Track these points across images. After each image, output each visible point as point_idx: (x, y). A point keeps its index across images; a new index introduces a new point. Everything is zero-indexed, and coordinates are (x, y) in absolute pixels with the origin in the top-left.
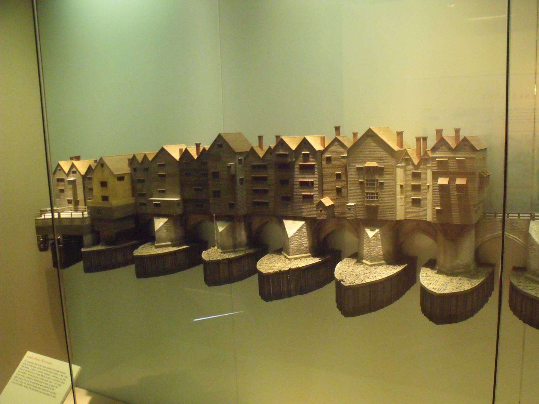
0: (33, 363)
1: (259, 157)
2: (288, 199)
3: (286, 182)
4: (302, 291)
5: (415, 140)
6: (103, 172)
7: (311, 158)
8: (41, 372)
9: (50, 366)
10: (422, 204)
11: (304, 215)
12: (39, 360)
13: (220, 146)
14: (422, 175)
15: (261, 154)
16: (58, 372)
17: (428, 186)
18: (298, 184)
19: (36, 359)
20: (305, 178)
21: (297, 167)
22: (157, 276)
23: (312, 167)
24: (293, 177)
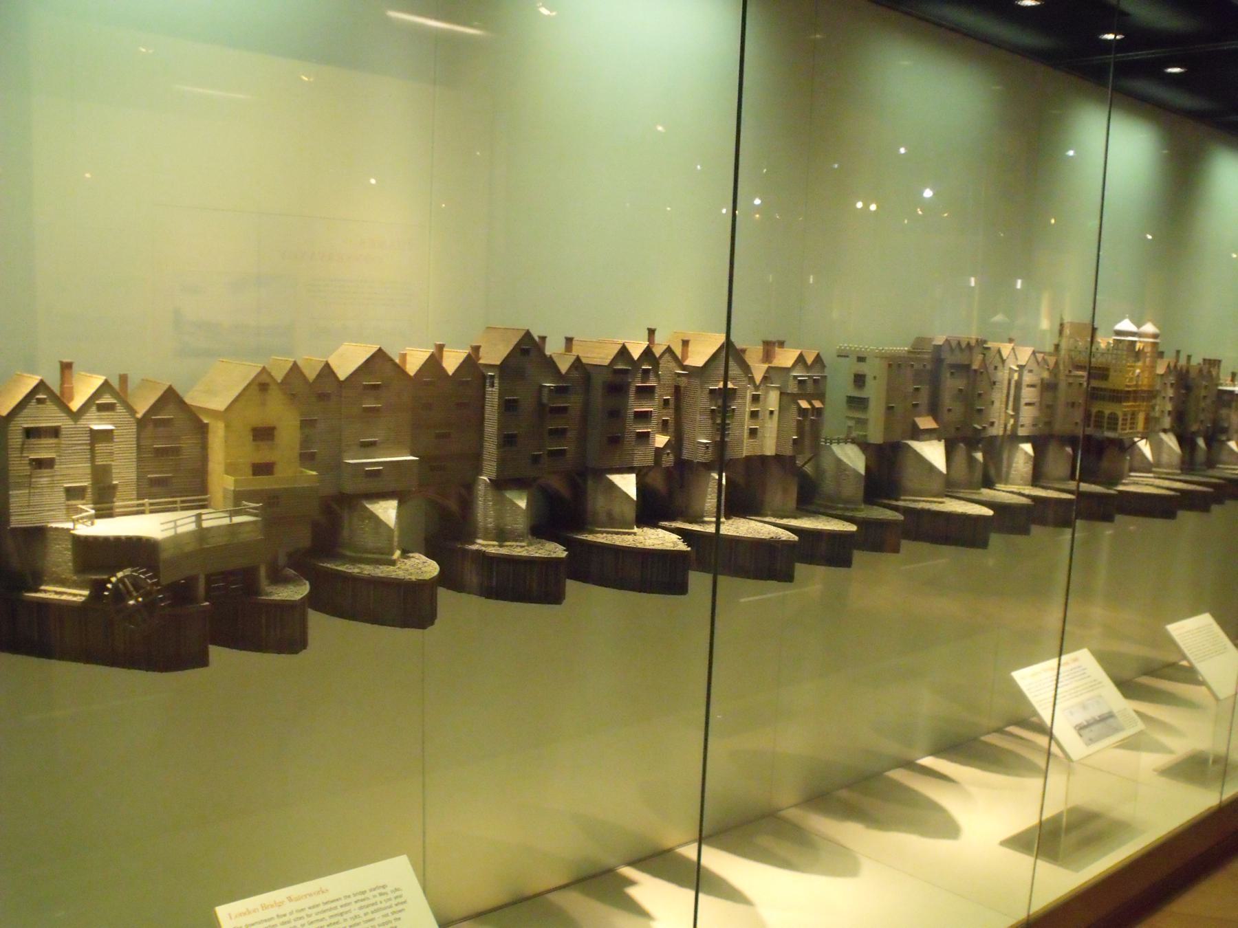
0: (272, 919)
1: (558, 371)
2: (615, 441)
3: (616, 414)
4: (644, 586)
5: (564, 341)
6: (263, 404)
7: (652, 377)
8: (322, 920)
9: (328, 897)
10: (759, 434)
11: (636, 464)
12: (279, 905)
13: (525, 352)
14: (762, 398)
15: (564, 367)
16: (364, 893)
17: (772, 412)
18: (632, 416)
19: (264, 907)
20: (642, 406)
21: (632, 390)
22: (229, 647)
23: (651, 390)
24: (626, 407)
